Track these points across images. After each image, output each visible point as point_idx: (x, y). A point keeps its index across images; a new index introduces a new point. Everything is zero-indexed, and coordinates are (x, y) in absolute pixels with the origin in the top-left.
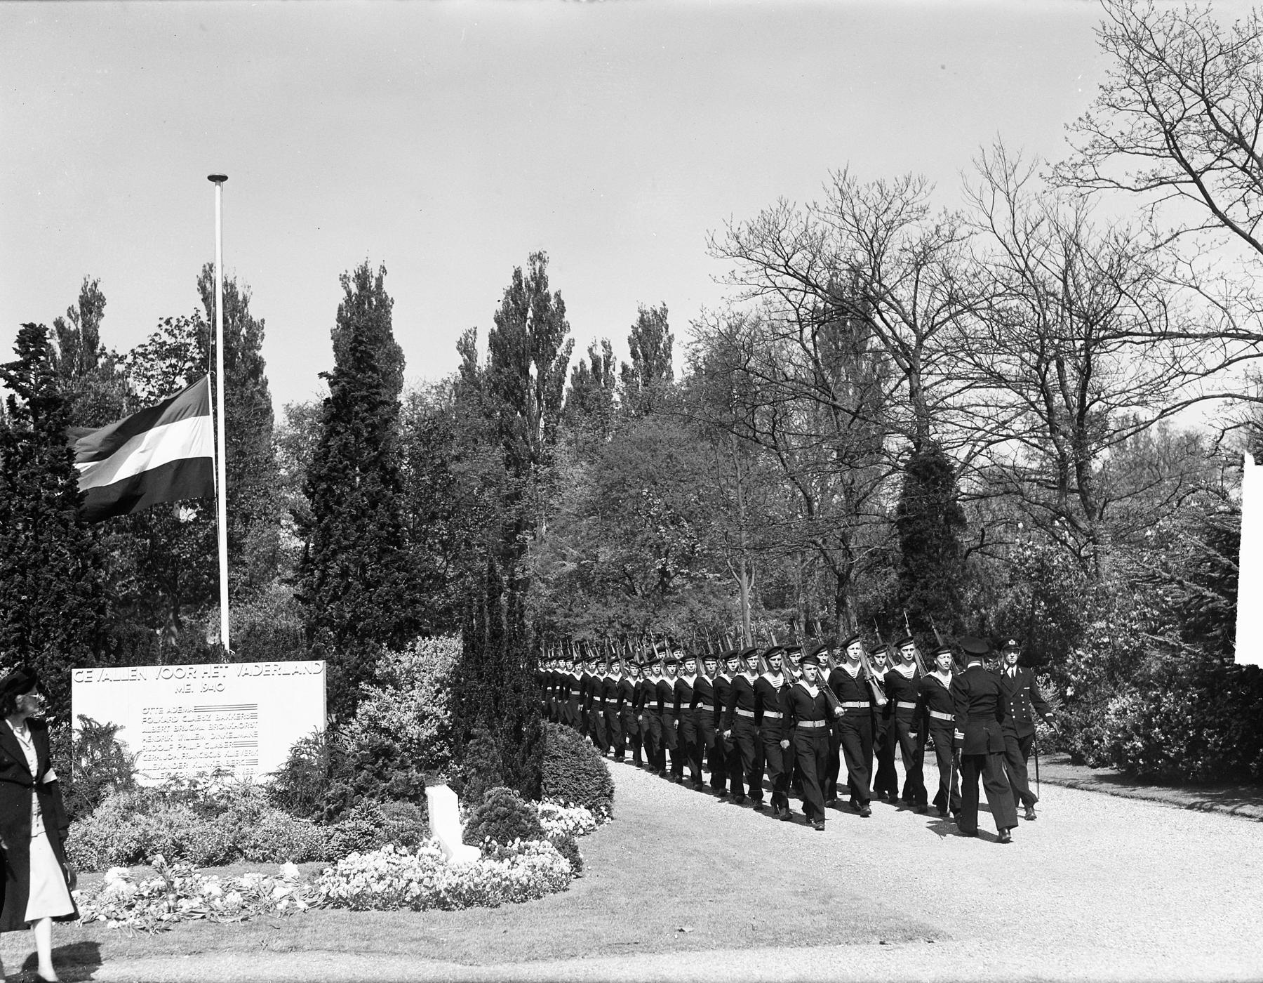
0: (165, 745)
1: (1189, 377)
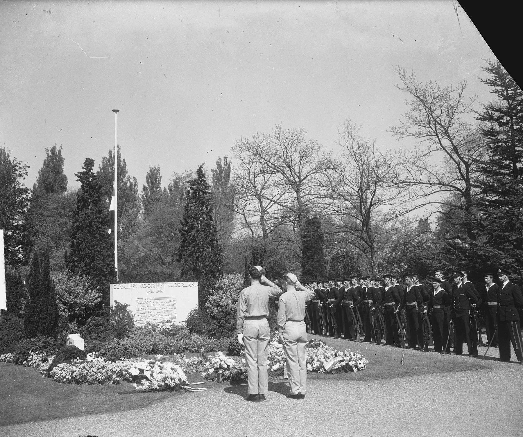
0: (144, 312)
1: (419, 197)
